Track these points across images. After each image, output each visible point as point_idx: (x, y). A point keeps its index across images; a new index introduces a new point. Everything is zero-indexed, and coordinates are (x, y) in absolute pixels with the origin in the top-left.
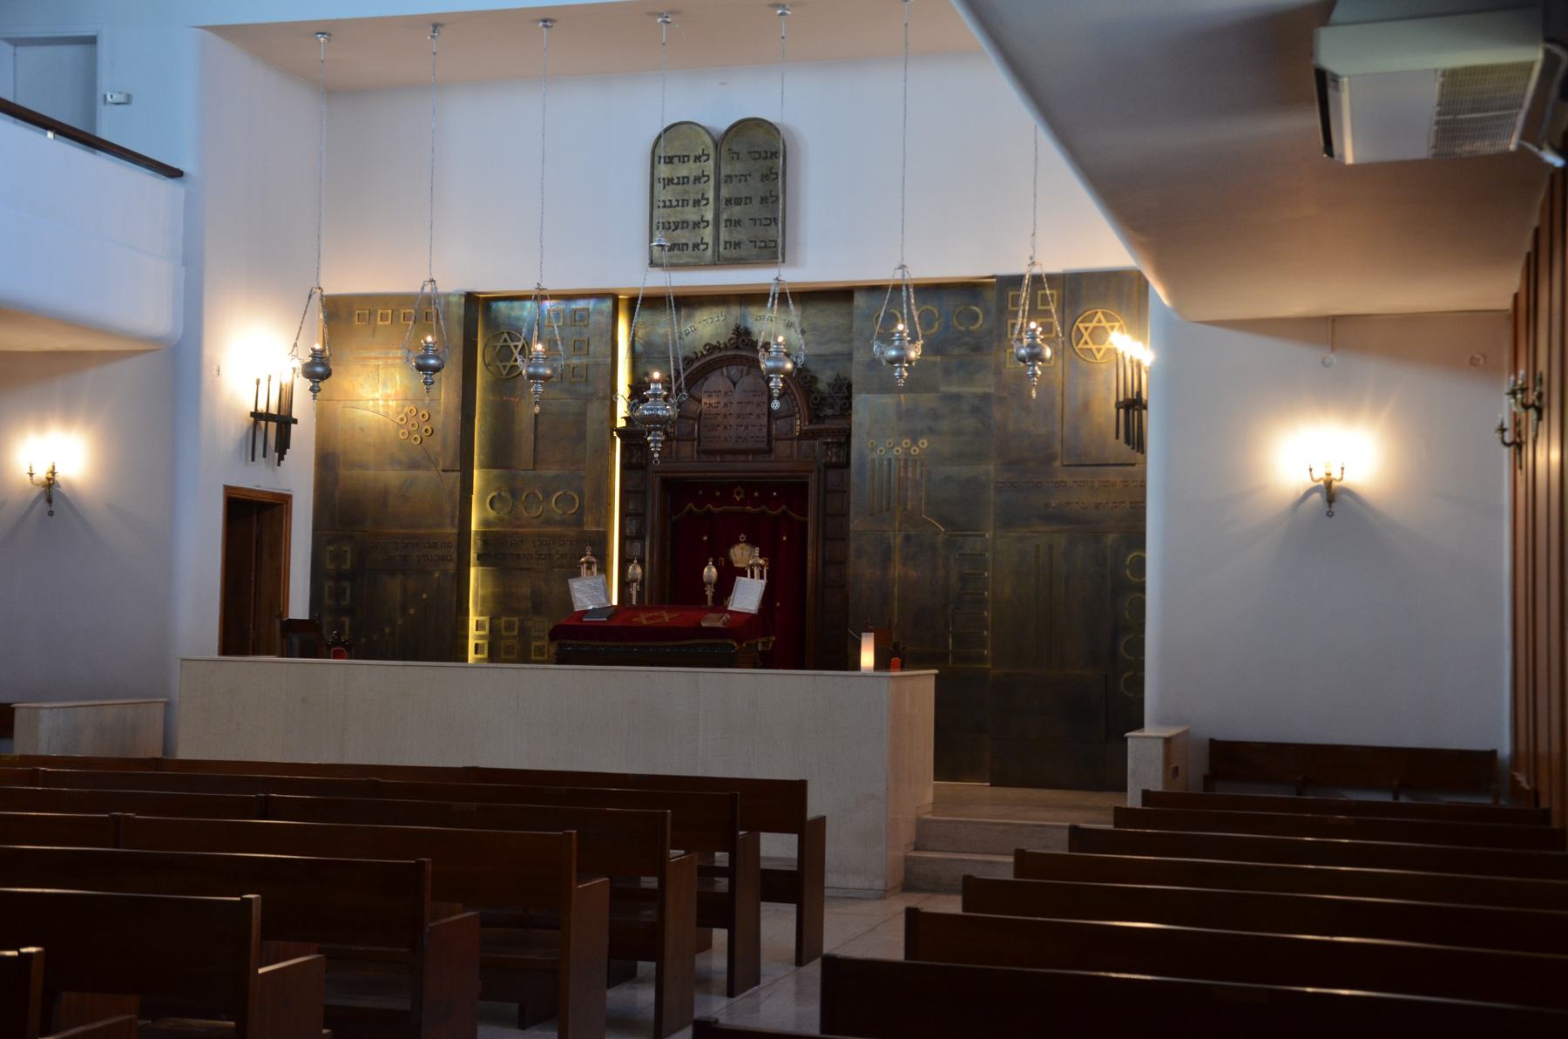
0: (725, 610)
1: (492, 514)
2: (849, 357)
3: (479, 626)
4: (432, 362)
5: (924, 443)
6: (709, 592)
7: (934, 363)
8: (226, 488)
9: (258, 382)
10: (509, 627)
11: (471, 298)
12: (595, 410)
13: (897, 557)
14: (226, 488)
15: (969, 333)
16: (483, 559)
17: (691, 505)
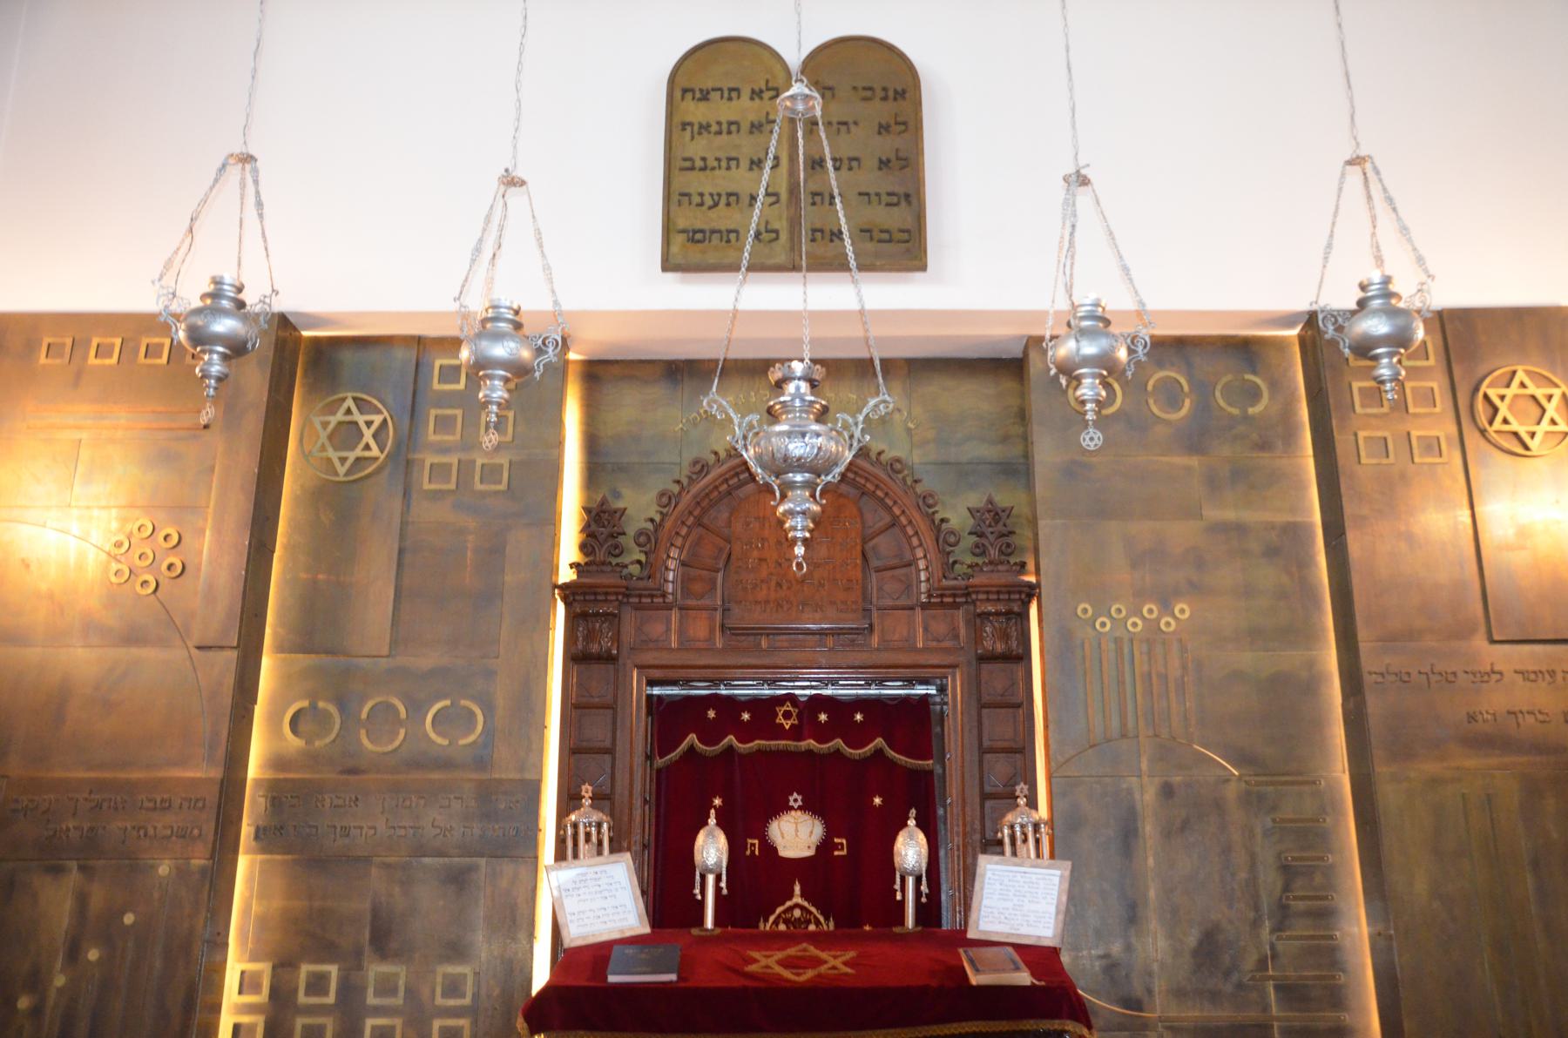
1: (294, 743)
7: (1188, 469)
10: (317, 984)
13: (1149, 829)
15: (1246, 418)
17: (692, 738)
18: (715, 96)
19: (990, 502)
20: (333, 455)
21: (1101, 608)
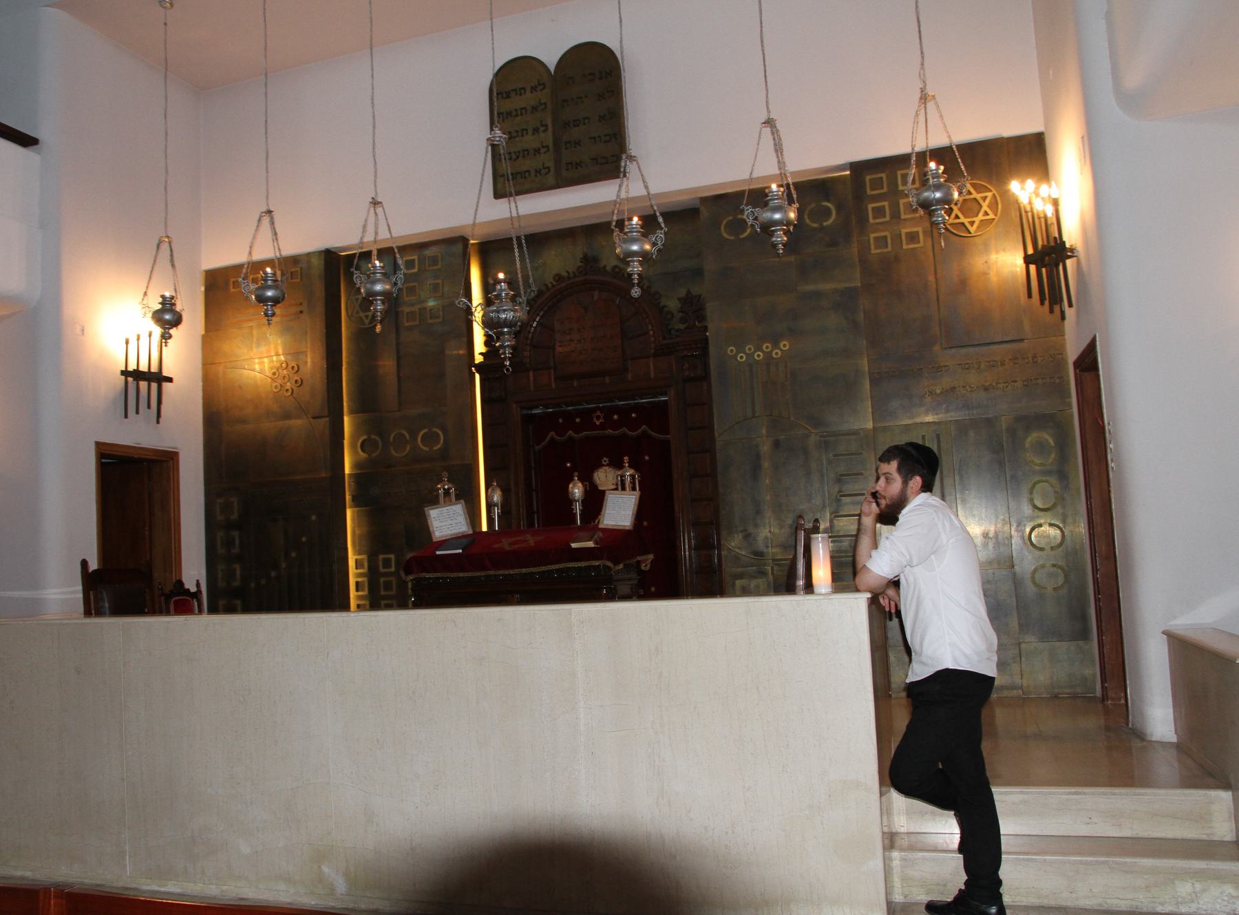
0: (596, 528)
2: (698, 273)
3: (358, 564)
4: (270, 293)
5: (785, 345)
6: (578, 508)
8: (98, 444)
9: (127, 342)
10: (387, 563)
11: (330, 257)
12: (455, 351)
13: (766, 464)
14: (98, 444)
15: (822, 229)
16: (357, 501)
17: (552, 434)
18: (513, 94)
19: (679, 299)
20: (362, 314)
21: (740, 349)
